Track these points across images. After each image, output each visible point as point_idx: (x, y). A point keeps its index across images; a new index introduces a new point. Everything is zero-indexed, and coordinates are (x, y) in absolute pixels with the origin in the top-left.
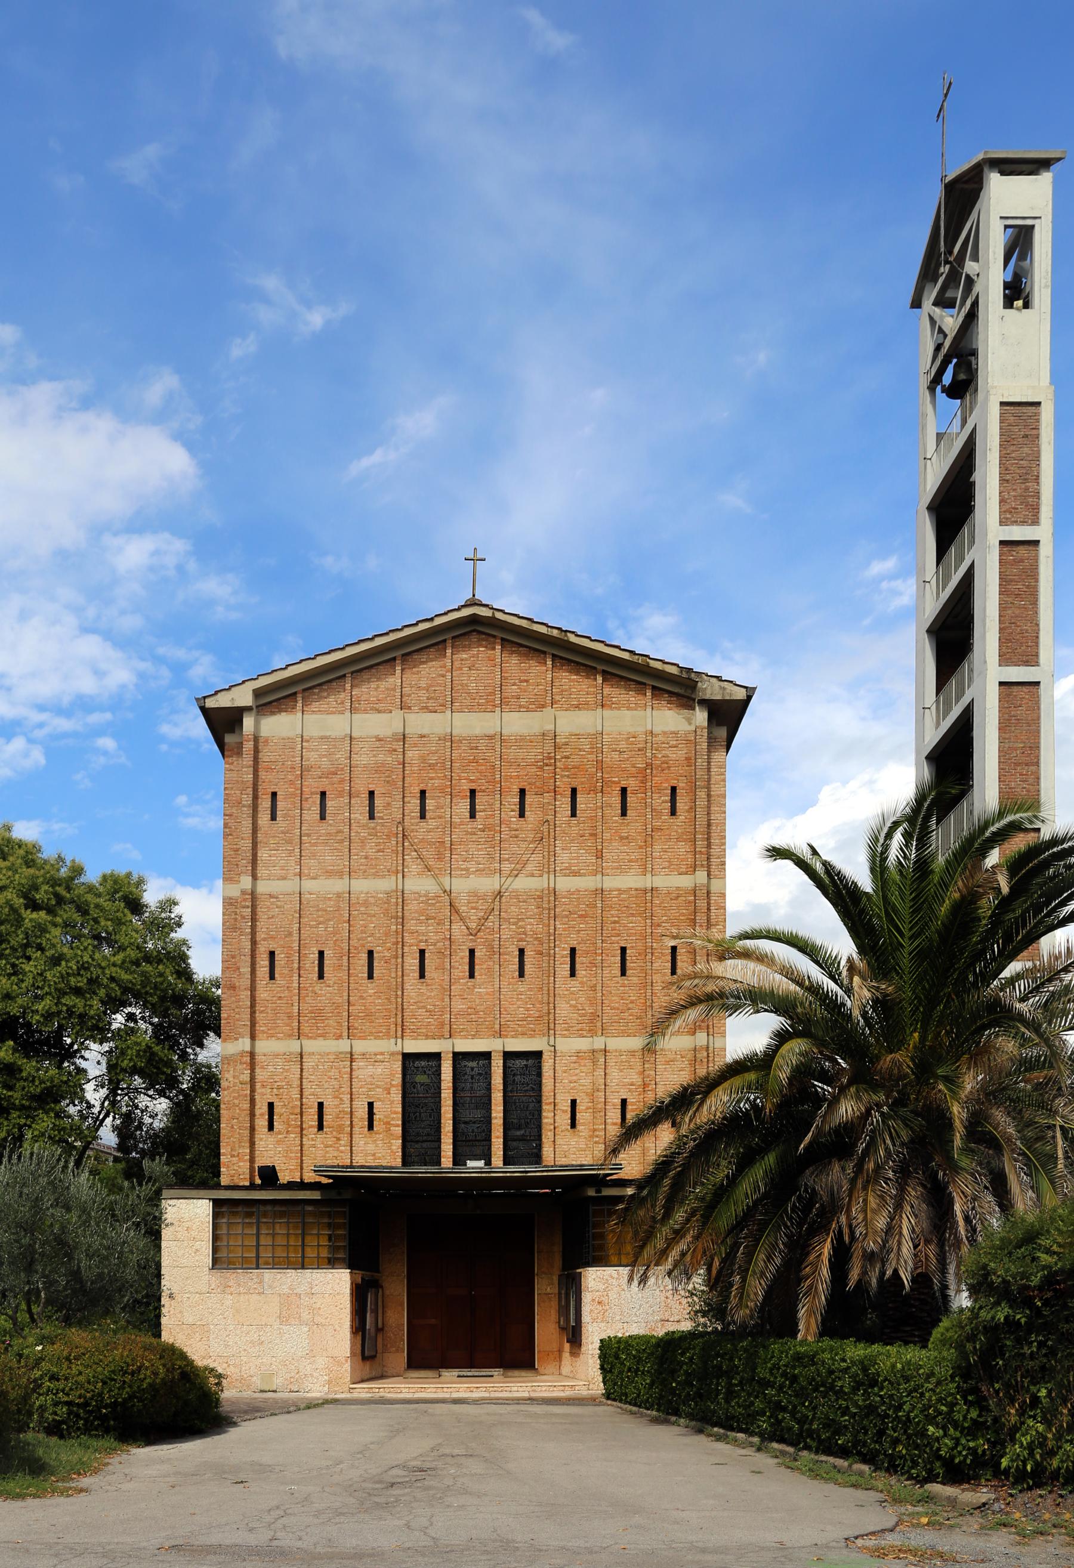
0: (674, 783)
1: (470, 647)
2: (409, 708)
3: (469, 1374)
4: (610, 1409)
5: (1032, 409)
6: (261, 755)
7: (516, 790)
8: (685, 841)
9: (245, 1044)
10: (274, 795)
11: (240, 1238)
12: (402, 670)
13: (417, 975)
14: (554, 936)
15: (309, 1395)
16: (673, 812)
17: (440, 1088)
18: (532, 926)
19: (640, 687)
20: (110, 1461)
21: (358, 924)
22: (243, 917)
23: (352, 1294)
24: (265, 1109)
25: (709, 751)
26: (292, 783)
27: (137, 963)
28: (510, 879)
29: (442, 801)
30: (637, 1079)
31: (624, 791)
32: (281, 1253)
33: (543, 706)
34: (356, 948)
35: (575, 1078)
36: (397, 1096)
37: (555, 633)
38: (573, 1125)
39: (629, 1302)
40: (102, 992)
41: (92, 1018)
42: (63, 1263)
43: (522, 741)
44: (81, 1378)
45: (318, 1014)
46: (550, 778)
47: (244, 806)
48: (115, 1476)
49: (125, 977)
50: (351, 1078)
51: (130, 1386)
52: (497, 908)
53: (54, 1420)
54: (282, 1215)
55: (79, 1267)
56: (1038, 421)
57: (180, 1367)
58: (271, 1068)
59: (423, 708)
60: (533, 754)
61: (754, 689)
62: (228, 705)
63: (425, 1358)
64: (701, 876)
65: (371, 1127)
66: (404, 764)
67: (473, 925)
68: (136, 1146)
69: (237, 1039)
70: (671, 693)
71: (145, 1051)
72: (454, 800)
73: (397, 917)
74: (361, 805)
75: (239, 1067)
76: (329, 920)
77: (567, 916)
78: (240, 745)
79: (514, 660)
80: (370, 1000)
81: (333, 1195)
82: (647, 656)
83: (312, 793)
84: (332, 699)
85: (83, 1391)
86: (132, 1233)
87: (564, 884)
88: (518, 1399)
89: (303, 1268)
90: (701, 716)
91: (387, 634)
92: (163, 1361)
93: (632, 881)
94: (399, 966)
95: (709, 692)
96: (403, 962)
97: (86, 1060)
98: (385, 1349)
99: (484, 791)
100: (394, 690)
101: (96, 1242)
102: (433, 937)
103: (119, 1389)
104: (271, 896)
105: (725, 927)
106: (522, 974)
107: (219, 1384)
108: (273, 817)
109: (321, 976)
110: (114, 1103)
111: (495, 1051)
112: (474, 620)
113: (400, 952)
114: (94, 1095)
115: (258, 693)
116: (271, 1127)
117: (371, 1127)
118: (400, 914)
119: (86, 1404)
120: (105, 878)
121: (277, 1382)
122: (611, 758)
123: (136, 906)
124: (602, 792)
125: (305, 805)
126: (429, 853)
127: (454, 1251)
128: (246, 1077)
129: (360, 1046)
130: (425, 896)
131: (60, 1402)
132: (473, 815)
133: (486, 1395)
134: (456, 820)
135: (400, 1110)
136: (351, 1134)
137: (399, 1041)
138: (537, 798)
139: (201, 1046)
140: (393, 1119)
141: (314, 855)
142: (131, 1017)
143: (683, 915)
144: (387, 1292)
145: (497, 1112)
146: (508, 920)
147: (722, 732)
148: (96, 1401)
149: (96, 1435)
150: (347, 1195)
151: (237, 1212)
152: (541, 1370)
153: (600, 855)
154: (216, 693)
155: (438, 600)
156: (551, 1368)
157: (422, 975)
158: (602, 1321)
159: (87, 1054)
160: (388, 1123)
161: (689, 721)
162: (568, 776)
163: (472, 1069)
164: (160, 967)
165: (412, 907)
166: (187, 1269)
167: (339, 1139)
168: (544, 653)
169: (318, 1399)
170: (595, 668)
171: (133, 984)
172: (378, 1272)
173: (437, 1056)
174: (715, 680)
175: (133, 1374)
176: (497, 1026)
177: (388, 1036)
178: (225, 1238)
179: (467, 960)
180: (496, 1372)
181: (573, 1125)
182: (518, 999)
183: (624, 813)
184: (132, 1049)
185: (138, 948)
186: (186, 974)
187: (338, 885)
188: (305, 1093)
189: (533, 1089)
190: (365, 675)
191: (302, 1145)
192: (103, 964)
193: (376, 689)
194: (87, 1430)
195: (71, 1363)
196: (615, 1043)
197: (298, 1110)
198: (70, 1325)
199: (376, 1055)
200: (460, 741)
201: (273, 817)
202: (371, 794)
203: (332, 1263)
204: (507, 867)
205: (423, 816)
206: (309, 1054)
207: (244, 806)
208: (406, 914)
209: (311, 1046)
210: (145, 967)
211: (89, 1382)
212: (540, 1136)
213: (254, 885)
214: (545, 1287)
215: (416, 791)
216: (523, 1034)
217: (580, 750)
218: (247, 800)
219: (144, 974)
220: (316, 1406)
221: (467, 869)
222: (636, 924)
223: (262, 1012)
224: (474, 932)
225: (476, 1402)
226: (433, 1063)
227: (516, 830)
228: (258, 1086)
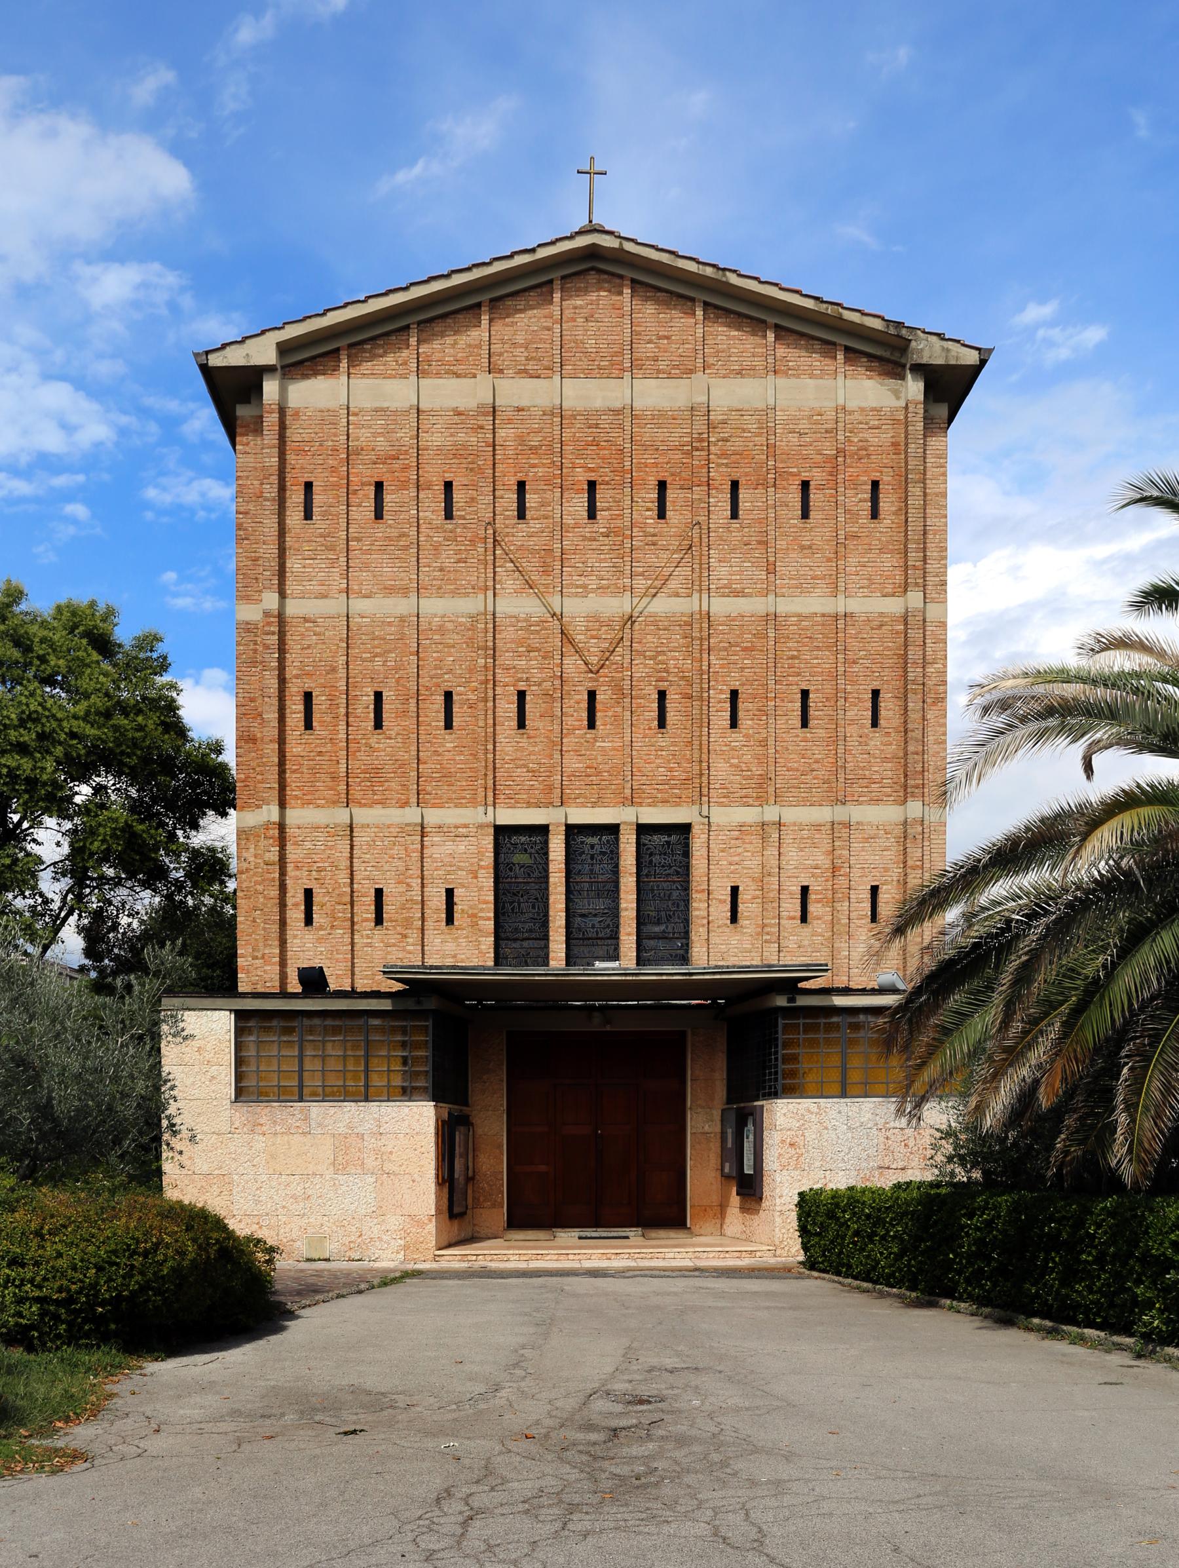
0: (875, 476)
1: (586, 291)
2: (501, 371)
3: (605, 1234)
4: (820, 1286)
6: (288, 433)
7: (653, 482)
8: (891, 552)
9: (272, 812)
10: (309, 486)
11: (275, 1061)
12: (491, 320)
13: (514, 723)
14: (708, 674)
15: (377, 1265)
16: (875, 514)
17: (546, 871)
18: (677, 661)
19: (828, 348)
20: (115, 1388)
21: (431, 656)
22: (267, 647)
23: (437, 1134)
24: (300, 897)
25: (925, 436)
26: (333, 469)
27: (108, 715)
28: (646, 600)
29: (548, 495)
30: (824, 861)
31: (805, 485)
32: (334, 1081)
33: (691, 371)
34: (428, 689)
35: (737, 859)
36: (487, 881)
37: (709, 271)
38: (734, 918)
39: (838, 1139)
40: (59, 751)
41: (45, 784)
42: (25, 1093)
43: (660, 417)
44: (60, 1262)
45: (375, 774)
46: (702, 467)
47: (266, 500)
48: (129, 1421)
49: (91, 731)
50: (422, 858)
51: (142, 1273)
52: (627, 637)
53: (17, 1324)
54: (336, 1030)
55: (50, 1099)
57: (217, 1241)
58: (308, 845)
59: (520, 372)
60: (678, 435)
61: (990, 351)
62: (241, 362)
63: (533, 1212)
64: (915, 598)
65: (450, 920)
66: (494, 446)
67: (594, 660)
68: (110, 951)
69: (259, 807)
70: (871, 357)
71: (123, 830)
72: (566, 495)
73: (486, 648)
74: (433, 502)
75: (263, 843)
76: (390, 652)
77: (725, 649)
78: (260, 419)
79: (650, 309)
80: (448, 756)
81: (410, 1004)
83: (363, 484)
84: (389, 358)
85: (65, 1282)
86: (132, 1051)
87: (721, 606)
88: (680, 1269)
89: (367, 1100)
90: (914, 388)
91: (468, 269)
92: (191, 1235)
93: (817, 603)
94: (490, 712)
96: (495, 707)
97: (39, 844)
98: (477, 1204)
99: (607, 484)
100: (479, 346)
101: (74, 1063)
102: (537, 675)
103: (124, 1277)
104: (306, 620)
105: (945, 666)
106: (662, 723)
107: (270, 1261)
108: (308, 515)
109: (378, 724)
110: (79, 898)
111: (625, 823)
112: (593, 254)
113: (490, 694)
114: (52, 887)
115: (284, 349)
116: (309, 921)
117: (450, 920)
118: (490, 644)
119: (70, 1300)
120: (59, 609)
121: (331, 1248)
122: (786, 441)
123: (103, 644)
124: (775, 486)
125: (354, 500)
126: (531, 565)
127: (582, 1078)
128: (273, 855)
129: (434, 816)
130: (526, 620)
131: (27, 1299)
132: (592, 514)
133: (633, 1264)
134: (568, 520)
135: (492, 898)
136: (423, 930)
137: (490, 809)
138: (682, 494)
139: (195, 826)
140: (482, 910)
141: (366, 566)
142: (99, 789)
143: (888, 648)
144: (479, 1131)
145: (627, 902)
146: (642, 654)
147: (942, 410)
148: (87, 1296)
149: (86, 1346)
150: (431, 1004)
151: (270, 1027)
152: (696, 1229)
153: (771, 569)
154: (224, 346)
155: (545, 223)
156: (709, 1226)
157: (521, 724)
158: (795, 1169)
159: (39, 834)
160: (474, 916)
161: (897, 394)
162: (726, 465)
163: (592, 847)
164: (140, 719)
165: (507, 635)
166: (199, 1103)
167: (405, 936)
168: (693, 300)
169: (393, 1271)
170: (764, 322)
171: (103, 742)
172: (467, 1105)
173: (543, 830)
174: (934, 339)
175: (146, 1254)
176: (628, 792)
177: (473, 802)
178: (253, 1061)
179: (585, 705)
180: (631, 1232)
181: (734, 918)
183: (805, 515)
184: (105, 826)
185: (107, 695)
186: (178, 730)
187: (403, 606)
188: (357, 877)
189: (678, 873)
190: (438, 327)
191: (353, 944)
192: (59, 715)
193: (453, 346)
194: (73, 1338)
195: (43, 1238)
196: (790, 814)
197: (348, 899)
198: (37, 1184)
199: (457, 827)
200: (574, 417)
201: (308, 515)
202: (448, 486)
203: (407, 1093)
204: (640, 583)
205: (521, 514)
206: (363, 826)
207: (266, 500)
208: (499, 644)
209: (363, 815)
210: (120, 720)
211: (74, 1268)
212: (686, 934)
213: (282, 605)
214: (703, 1124)
215: (512, 481)
216: (665, 802)
217: (744, 430)
218: (271, 491)
219: (116, 728)
220: (394, 1281)
221: (585, 586)
222: (824, 661)
223: (294, 772)
224: (594, 669)
225: (621, 1274)
226: (538, 839)
228: (290, 868)
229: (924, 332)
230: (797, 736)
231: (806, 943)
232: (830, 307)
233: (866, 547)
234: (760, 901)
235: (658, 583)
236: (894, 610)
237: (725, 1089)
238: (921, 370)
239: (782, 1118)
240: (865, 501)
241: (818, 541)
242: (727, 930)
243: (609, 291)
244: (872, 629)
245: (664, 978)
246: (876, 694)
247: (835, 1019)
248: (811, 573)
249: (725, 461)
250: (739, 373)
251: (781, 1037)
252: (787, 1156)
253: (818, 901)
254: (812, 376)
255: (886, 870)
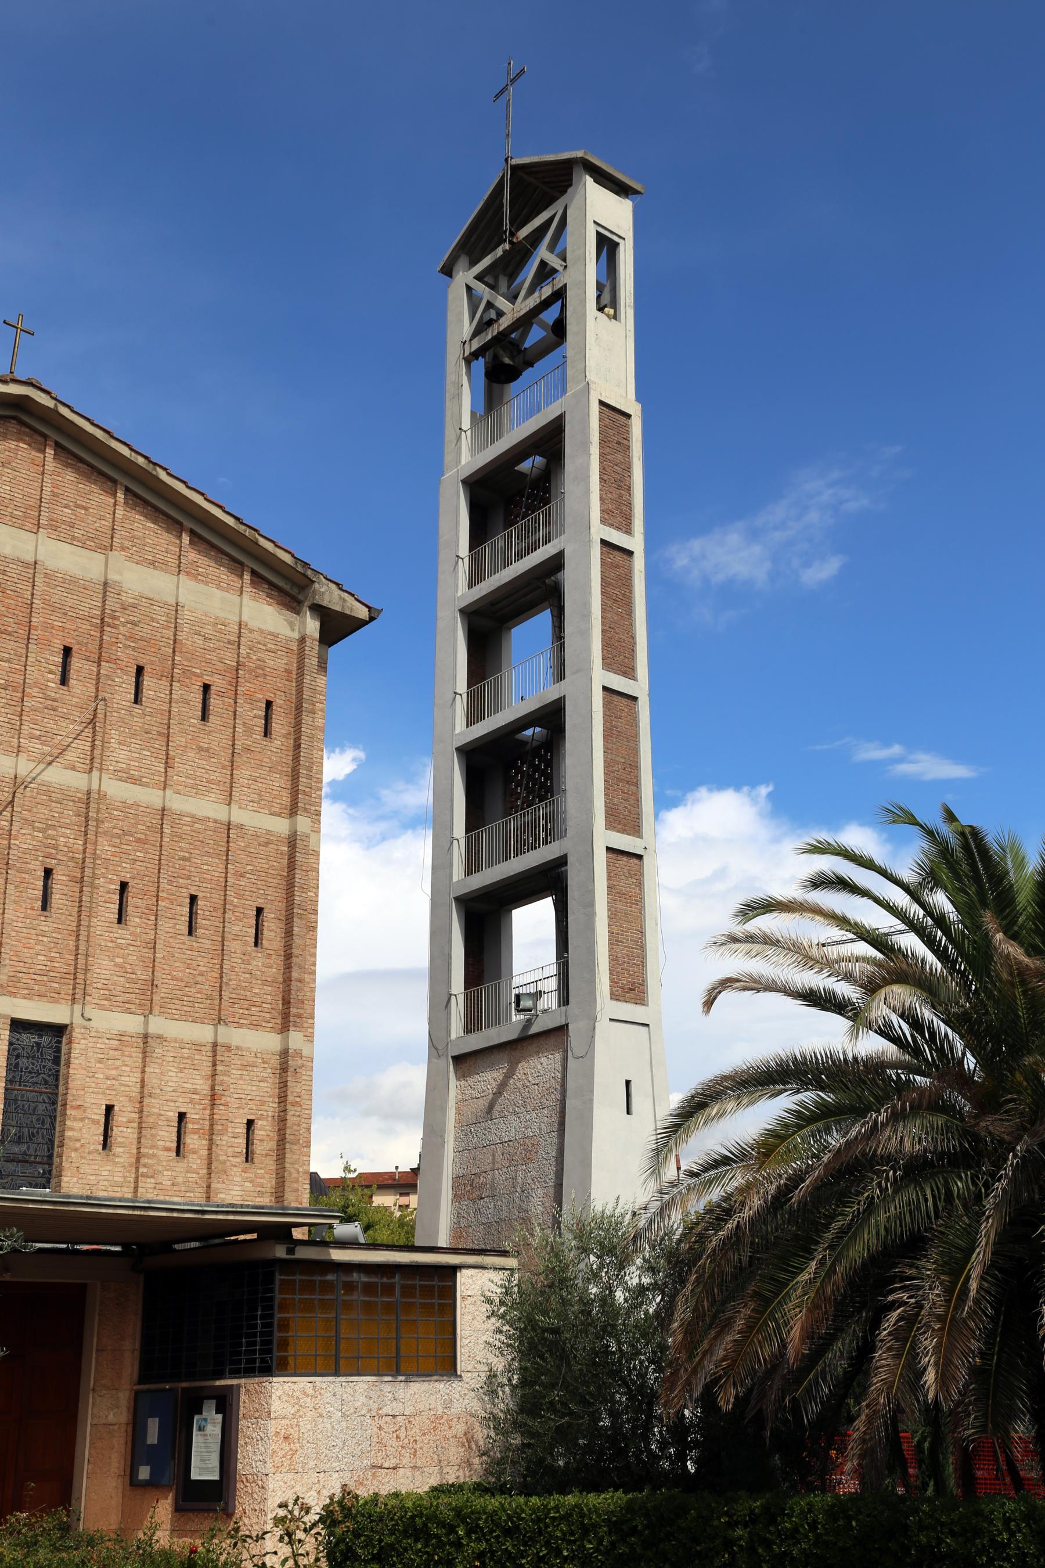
0: (270, 696)
5: (623, 419)
7: (58, 646)
16: (267, 732)
18: (69, 839)
19: (237, 566)
28: (42, 766)
31: (206, 688)
35: (114, 1072)
37: (141, 461)
43: (71, 582)
56: (628, 432)
70: (272, 585)
77: (119, 837)
82: (256, 530)
87: (115, 789)
90: (312, 626)
93: (210, 808)
95: (327, 598)
105: (317, 896)
143: (272, 867)
158: (289, 1471)
162: (134, 649)
168: (115, 482)
170: (181, 524)
174: (333, 586)
182: (38, 942)
183: (204, 717)
189: (46, 1082)
214: (105, 1415)
217: (153, 620)
227: (54, 700)
229: (326, 578)
230: (184, 943)
231: (180, 1180)
232: (248, 530)
233: (258, 762)
234: (135, 1125)
235: (56, 752)
236: (280, 831)
237: (137, 1364)
238: (321, 611)
239: (277, 1403)
240: (259, 717)
241: (214, 746)
242: (98, 1157)
243: (29, 445)
244: (260, 845)
245: (175, 1215)
246: (259, 911)
247: (330, 1277)
248: (207, 776)
249: (132, 644)
250: (152, 564)
251: (278, 1297)
252: (280, 1454)
253: (195, 1132)
254: (219, 587)
255: (263, 1103)
